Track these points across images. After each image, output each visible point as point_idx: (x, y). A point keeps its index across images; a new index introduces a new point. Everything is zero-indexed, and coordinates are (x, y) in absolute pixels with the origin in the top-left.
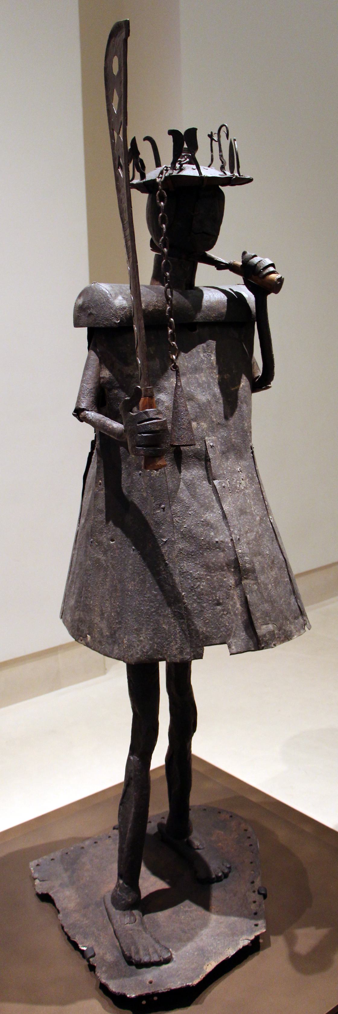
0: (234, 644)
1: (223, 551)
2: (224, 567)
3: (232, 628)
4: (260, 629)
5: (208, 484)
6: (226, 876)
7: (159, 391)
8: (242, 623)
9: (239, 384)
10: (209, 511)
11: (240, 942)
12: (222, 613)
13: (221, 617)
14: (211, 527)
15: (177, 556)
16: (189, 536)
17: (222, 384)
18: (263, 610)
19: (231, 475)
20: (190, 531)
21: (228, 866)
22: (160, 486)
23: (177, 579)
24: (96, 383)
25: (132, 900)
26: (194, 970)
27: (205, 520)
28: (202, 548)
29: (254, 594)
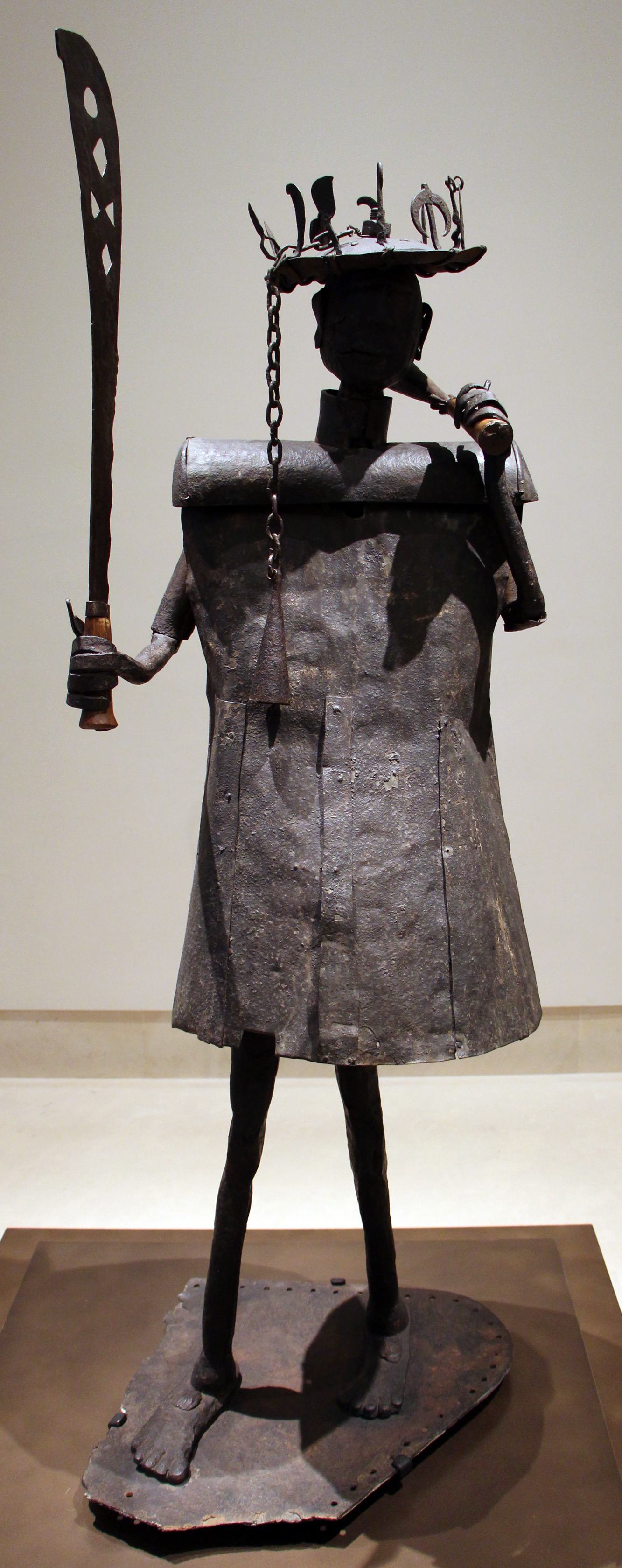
0: (285, 1039)
1: (304, 885)
2: (298, 911)
3: (289, 1013)
4: (329, 1028)
5: (315, 772)
6: (383, 1415)
7: (260, 611)
8: (308, 1010)
9: (438, 610)
10: (299, 817)
11: (287, 1513)
12: (278, 984)
13: (276, 991)
14: (294, 842)
15: (233, 878)
16: (257, 850)
17: (396, 612)
18: (346, 999)
19: (367, 764)
20: (259, 841)
21: (398, 1403)
22: (230, 762)
23: (227, 914)
24: (178, 592)
25: (208, 1379)
26: (190, 1511)
27: (287, 830)
28: (271, 873)
29: (338, 969)
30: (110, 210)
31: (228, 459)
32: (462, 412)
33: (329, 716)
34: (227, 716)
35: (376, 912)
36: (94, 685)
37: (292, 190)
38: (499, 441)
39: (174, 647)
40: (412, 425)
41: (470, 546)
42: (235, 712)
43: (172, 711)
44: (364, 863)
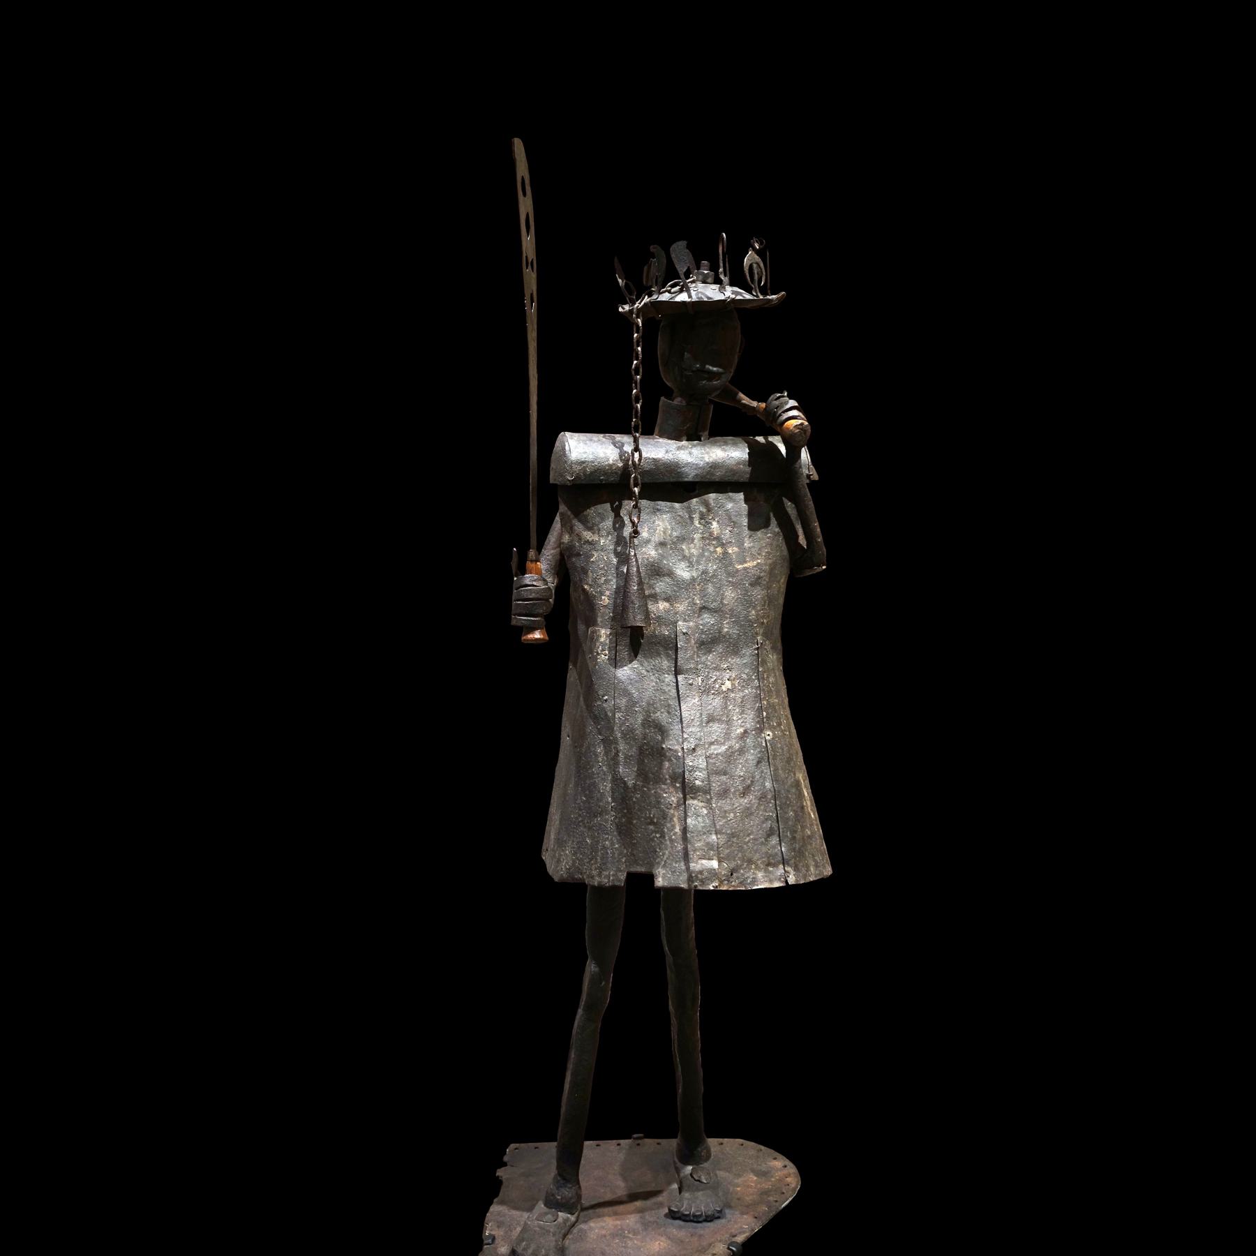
1: (670, 760)
29: (700, 819)
33: (681, 638)
35: (724, 778)
44: (712, 743)
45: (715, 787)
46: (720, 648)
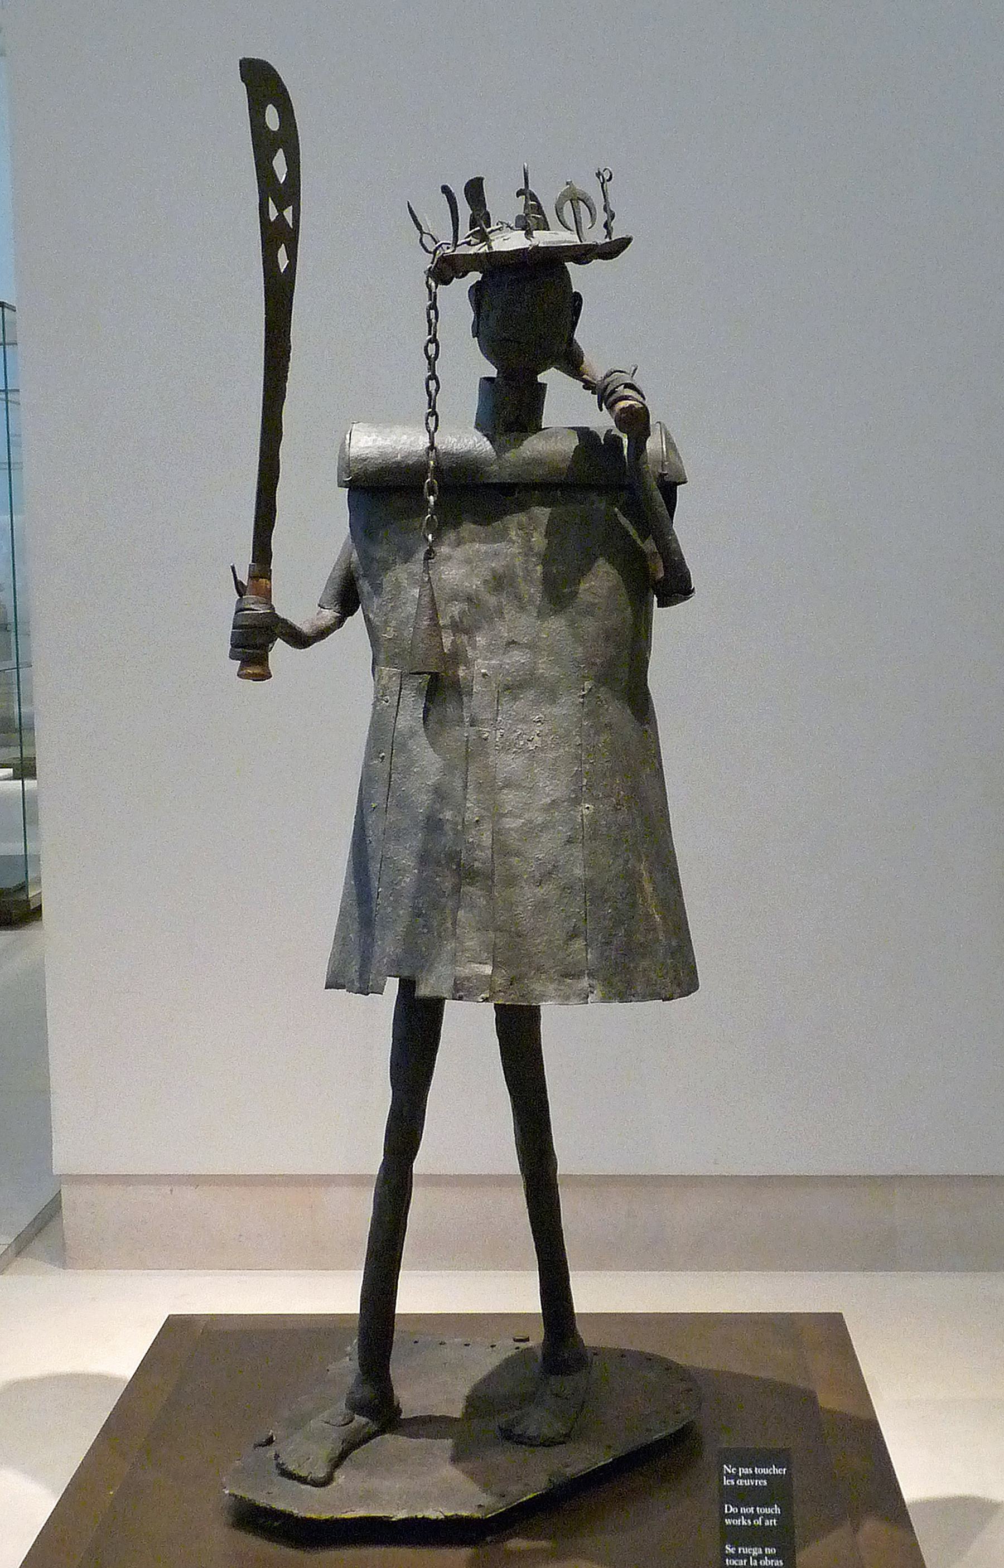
30: (288, 213)
31: (388, 443)
32: (605, 396)
34: (383, 682)
36: (254, 641)
37: (445, 190)
38: (636, 422)
39: (339, 622)
40: (567, 409)
41: (624, 521)
42: (390, 678)
43: (336, 683)
45: (499, 870)
46: (531, 694)
